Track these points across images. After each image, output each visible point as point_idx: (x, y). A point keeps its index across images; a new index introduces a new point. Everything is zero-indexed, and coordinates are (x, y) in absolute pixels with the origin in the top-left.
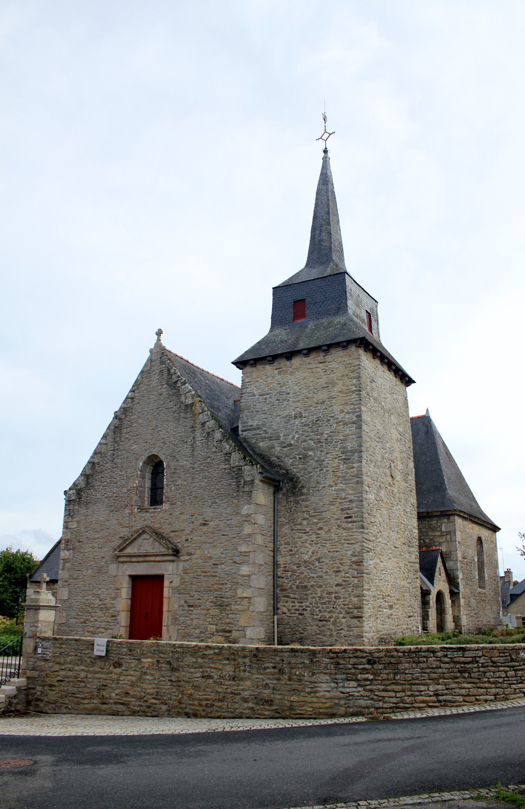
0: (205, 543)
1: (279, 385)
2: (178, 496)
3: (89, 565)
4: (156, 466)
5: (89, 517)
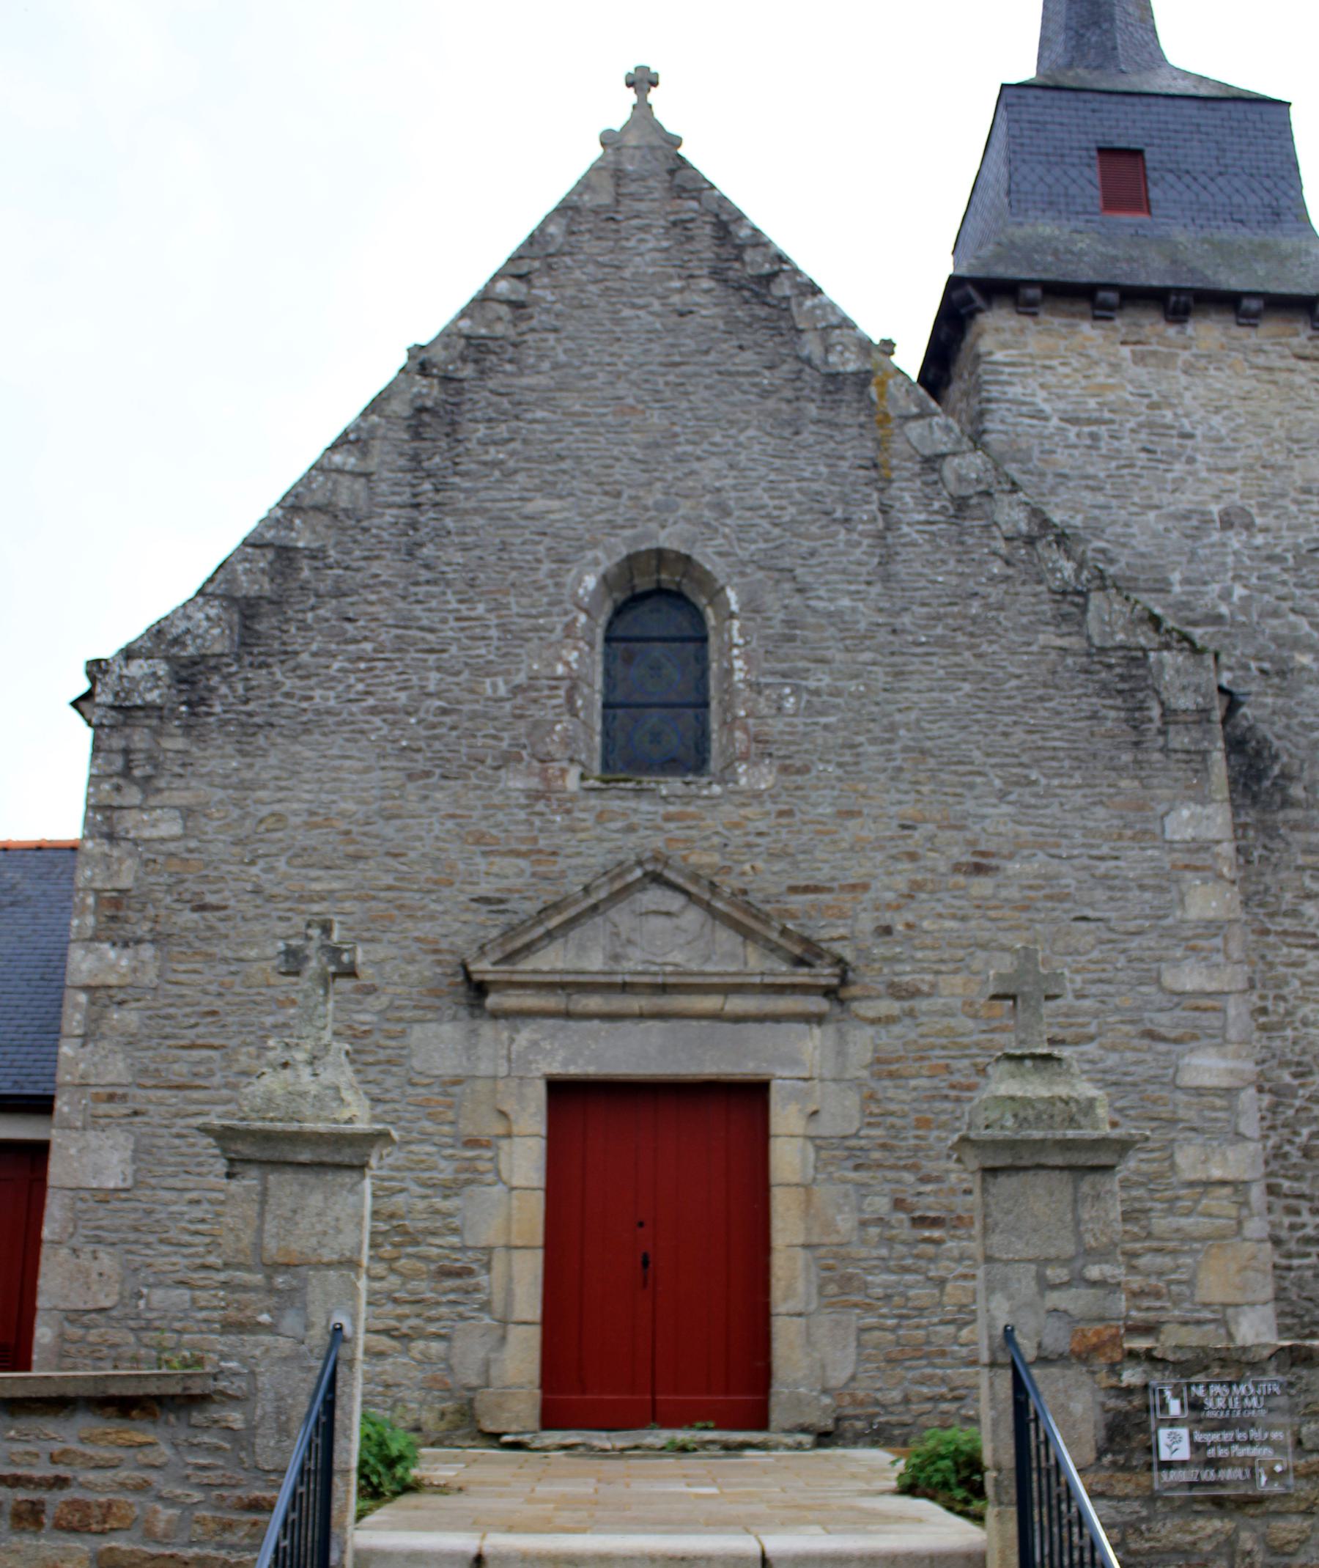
0: (984, 946)
1: (1146, 401)
2: (820, 736)
3: (269, 1020)
4: (657, 607)
5: (261, 794)
